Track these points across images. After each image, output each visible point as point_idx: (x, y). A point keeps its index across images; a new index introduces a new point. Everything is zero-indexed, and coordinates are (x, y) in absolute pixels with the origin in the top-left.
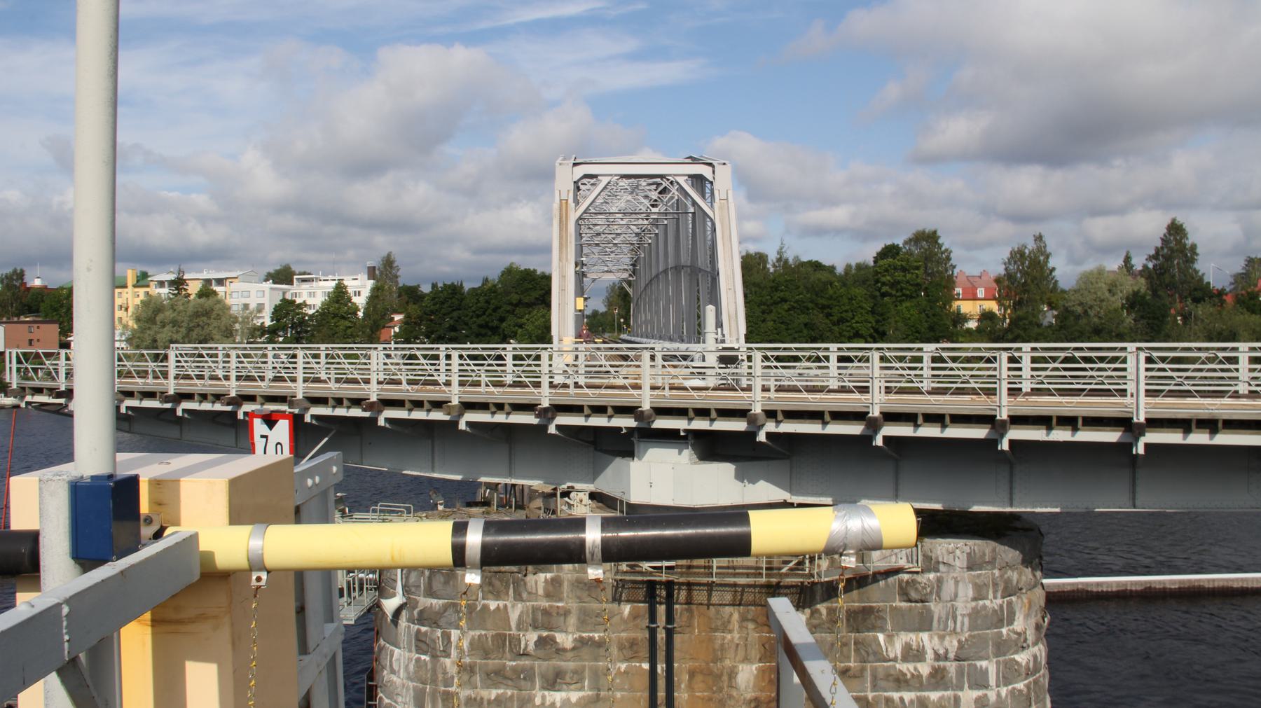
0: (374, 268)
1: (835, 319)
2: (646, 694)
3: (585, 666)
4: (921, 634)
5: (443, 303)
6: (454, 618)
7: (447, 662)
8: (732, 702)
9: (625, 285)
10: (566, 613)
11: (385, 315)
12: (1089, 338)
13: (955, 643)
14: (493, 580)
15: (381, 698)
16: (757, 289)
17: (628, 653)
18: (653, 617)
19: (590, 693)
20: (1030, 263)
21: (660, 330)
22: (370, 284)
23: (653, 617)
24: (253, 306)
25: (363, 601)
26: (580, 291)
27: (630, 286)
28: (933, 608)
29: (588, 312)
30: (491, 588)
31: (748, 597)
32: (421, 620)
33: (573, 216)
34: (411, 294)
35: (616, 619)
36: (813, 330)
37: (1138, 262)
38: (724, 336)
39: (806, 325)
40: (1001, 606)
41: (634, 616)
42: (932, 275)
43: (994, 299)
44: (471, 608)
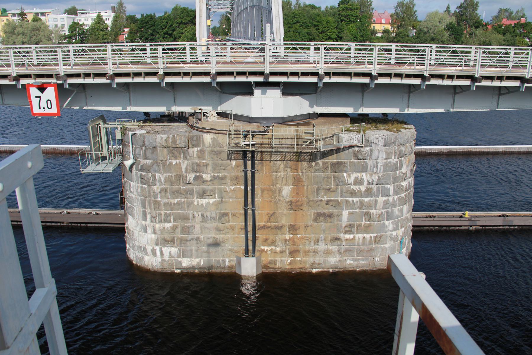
0: (114, 7)
1: (320, 31)
2: (243, 200)
3: (216, 188)
4: (362, 174)
5: (146, 23)
6: (157, 168)
7: (155, 187)
8: (280, 202)
9: (228, 15)
10: (207, 165)
11: (121, 29)
13: (377, 177)
14: (174, 151)
15: (127, 203)
16: (286, 17)
17: (235, 182)
18: (245, 166)
19: (218, 199)
20: (406, 8)
21: (244, 35)
22: (113, 14)
23: (245, 166)
24: (59, 25)
25: (116, 161)
26: (208, 17)
27: (230, 15)
28: (368, 162)
29: (212, 27)
30: (173, 155)
31: (288, 157)
32: (142, 170)
34: (132, 19)
35: (230, 167)
37: (453, 9)
38: (274, 38)
39: (307, 33)
40: (397, 162)
41: (237, 166)
42: (363, 12)
43: (390, 24)
44: (164, 164)
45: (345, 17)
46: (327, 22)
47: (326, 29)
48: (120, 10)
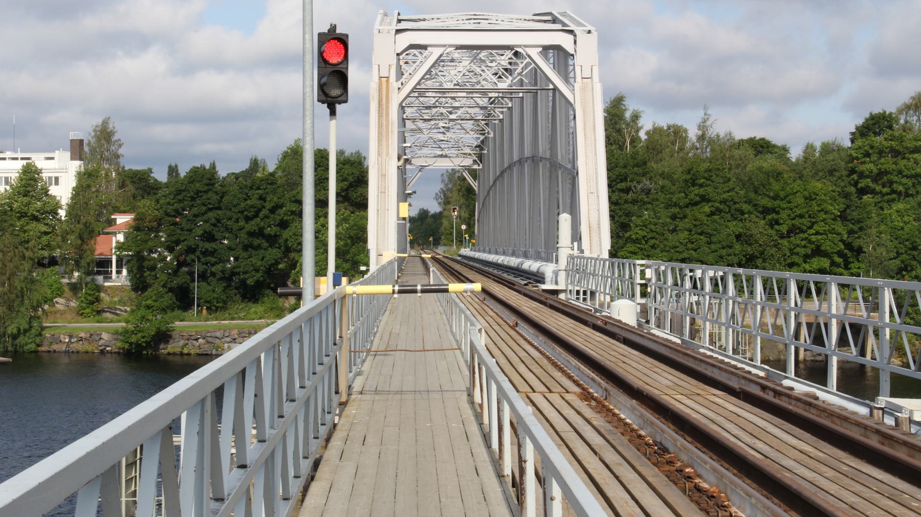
0: (81, 141)
1: (784, 229)
5: (193, 199)
9: (466, 175)
12: (288, 250)
22: (76, 166)
33: (396, 99)
36: (750, 245)
39: (738, 237)
45: (875, 180)
46: (809, 199)
47: (806, 221)
48: (102, 153)
